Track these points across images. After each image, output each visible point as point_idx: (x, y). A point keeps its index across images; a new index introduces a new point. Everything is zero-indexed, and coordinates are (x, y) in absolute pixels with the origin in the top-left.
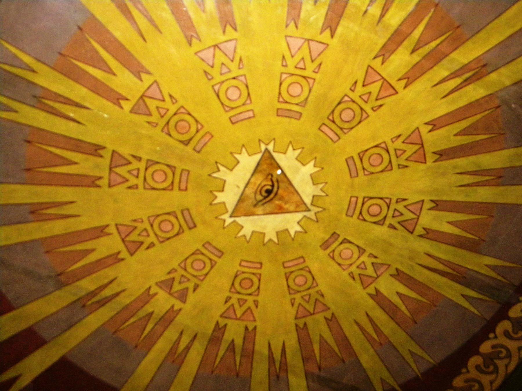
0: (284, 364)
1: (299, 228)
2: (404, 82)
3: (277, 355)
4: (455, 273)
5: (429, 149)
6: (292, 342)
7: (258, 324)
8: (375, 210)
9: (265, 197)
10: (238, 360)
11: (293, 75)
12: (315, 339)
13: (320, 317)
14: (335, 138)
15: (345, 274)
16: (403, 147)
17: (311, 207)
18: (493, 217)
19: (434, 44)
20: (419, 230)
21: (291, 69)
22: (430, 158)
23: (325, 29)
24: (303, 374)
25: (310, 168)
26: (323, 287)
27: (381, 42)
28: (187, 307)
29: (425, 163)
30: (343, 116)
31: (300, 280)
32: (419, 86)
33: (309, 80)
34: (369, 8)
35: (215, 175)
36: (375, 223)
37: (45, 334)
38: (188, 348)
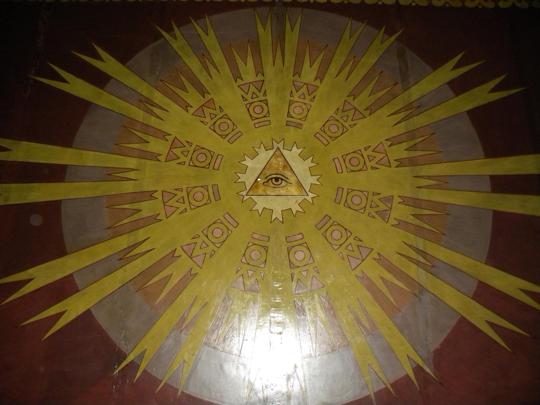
0: (405, 108)
1: (295, 148)
2: (167, 137)
3: (402, 115)
4: (279, 43)
5: (203, 101)
6: (386, 110)
7: (383, 140)
8: (258, 110)
9: (282, 179)
10: (420, 139)
11: (189, 202)
12: (373, 98)
13: (355, 103)
14: (220, 157)
15: (313, 104)
16: (208, 116)
17: (275, 148)
18: (230, 44)
19: (139, 134)
20: (260, 77)
21: (187, 205)
22: (208, 97)
23: (154, 197)
24: (407, 92)
25: (248, 162)
26: (331, 113)
27: (149, 162)
28: (395, 193)
29: (213, 98)
30: (203, 160)
31: (334, 129)
32: (165, 127)
33: (189, 191)
34: (251, 264)
35: (281, 220)
36: (267, 105)
37: (474, 286)
38: (429, 177)
